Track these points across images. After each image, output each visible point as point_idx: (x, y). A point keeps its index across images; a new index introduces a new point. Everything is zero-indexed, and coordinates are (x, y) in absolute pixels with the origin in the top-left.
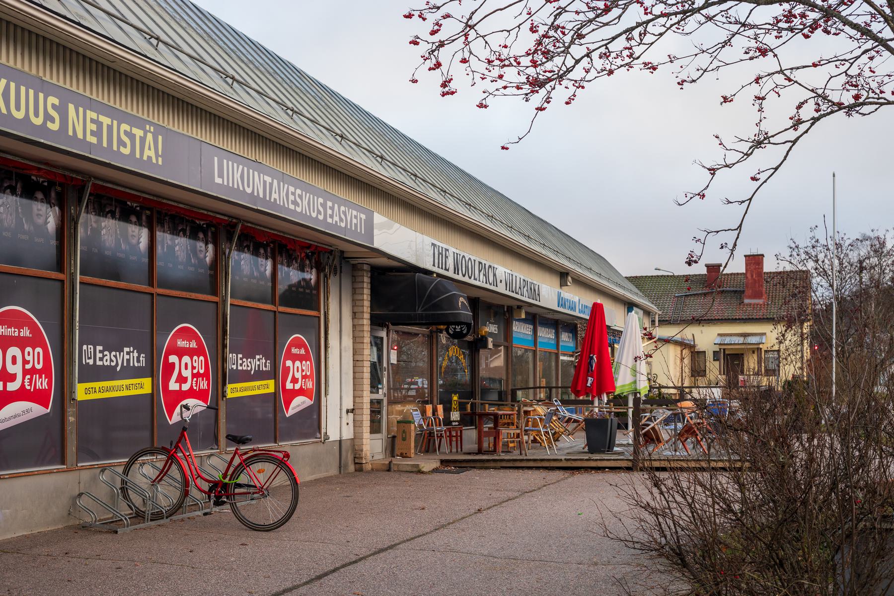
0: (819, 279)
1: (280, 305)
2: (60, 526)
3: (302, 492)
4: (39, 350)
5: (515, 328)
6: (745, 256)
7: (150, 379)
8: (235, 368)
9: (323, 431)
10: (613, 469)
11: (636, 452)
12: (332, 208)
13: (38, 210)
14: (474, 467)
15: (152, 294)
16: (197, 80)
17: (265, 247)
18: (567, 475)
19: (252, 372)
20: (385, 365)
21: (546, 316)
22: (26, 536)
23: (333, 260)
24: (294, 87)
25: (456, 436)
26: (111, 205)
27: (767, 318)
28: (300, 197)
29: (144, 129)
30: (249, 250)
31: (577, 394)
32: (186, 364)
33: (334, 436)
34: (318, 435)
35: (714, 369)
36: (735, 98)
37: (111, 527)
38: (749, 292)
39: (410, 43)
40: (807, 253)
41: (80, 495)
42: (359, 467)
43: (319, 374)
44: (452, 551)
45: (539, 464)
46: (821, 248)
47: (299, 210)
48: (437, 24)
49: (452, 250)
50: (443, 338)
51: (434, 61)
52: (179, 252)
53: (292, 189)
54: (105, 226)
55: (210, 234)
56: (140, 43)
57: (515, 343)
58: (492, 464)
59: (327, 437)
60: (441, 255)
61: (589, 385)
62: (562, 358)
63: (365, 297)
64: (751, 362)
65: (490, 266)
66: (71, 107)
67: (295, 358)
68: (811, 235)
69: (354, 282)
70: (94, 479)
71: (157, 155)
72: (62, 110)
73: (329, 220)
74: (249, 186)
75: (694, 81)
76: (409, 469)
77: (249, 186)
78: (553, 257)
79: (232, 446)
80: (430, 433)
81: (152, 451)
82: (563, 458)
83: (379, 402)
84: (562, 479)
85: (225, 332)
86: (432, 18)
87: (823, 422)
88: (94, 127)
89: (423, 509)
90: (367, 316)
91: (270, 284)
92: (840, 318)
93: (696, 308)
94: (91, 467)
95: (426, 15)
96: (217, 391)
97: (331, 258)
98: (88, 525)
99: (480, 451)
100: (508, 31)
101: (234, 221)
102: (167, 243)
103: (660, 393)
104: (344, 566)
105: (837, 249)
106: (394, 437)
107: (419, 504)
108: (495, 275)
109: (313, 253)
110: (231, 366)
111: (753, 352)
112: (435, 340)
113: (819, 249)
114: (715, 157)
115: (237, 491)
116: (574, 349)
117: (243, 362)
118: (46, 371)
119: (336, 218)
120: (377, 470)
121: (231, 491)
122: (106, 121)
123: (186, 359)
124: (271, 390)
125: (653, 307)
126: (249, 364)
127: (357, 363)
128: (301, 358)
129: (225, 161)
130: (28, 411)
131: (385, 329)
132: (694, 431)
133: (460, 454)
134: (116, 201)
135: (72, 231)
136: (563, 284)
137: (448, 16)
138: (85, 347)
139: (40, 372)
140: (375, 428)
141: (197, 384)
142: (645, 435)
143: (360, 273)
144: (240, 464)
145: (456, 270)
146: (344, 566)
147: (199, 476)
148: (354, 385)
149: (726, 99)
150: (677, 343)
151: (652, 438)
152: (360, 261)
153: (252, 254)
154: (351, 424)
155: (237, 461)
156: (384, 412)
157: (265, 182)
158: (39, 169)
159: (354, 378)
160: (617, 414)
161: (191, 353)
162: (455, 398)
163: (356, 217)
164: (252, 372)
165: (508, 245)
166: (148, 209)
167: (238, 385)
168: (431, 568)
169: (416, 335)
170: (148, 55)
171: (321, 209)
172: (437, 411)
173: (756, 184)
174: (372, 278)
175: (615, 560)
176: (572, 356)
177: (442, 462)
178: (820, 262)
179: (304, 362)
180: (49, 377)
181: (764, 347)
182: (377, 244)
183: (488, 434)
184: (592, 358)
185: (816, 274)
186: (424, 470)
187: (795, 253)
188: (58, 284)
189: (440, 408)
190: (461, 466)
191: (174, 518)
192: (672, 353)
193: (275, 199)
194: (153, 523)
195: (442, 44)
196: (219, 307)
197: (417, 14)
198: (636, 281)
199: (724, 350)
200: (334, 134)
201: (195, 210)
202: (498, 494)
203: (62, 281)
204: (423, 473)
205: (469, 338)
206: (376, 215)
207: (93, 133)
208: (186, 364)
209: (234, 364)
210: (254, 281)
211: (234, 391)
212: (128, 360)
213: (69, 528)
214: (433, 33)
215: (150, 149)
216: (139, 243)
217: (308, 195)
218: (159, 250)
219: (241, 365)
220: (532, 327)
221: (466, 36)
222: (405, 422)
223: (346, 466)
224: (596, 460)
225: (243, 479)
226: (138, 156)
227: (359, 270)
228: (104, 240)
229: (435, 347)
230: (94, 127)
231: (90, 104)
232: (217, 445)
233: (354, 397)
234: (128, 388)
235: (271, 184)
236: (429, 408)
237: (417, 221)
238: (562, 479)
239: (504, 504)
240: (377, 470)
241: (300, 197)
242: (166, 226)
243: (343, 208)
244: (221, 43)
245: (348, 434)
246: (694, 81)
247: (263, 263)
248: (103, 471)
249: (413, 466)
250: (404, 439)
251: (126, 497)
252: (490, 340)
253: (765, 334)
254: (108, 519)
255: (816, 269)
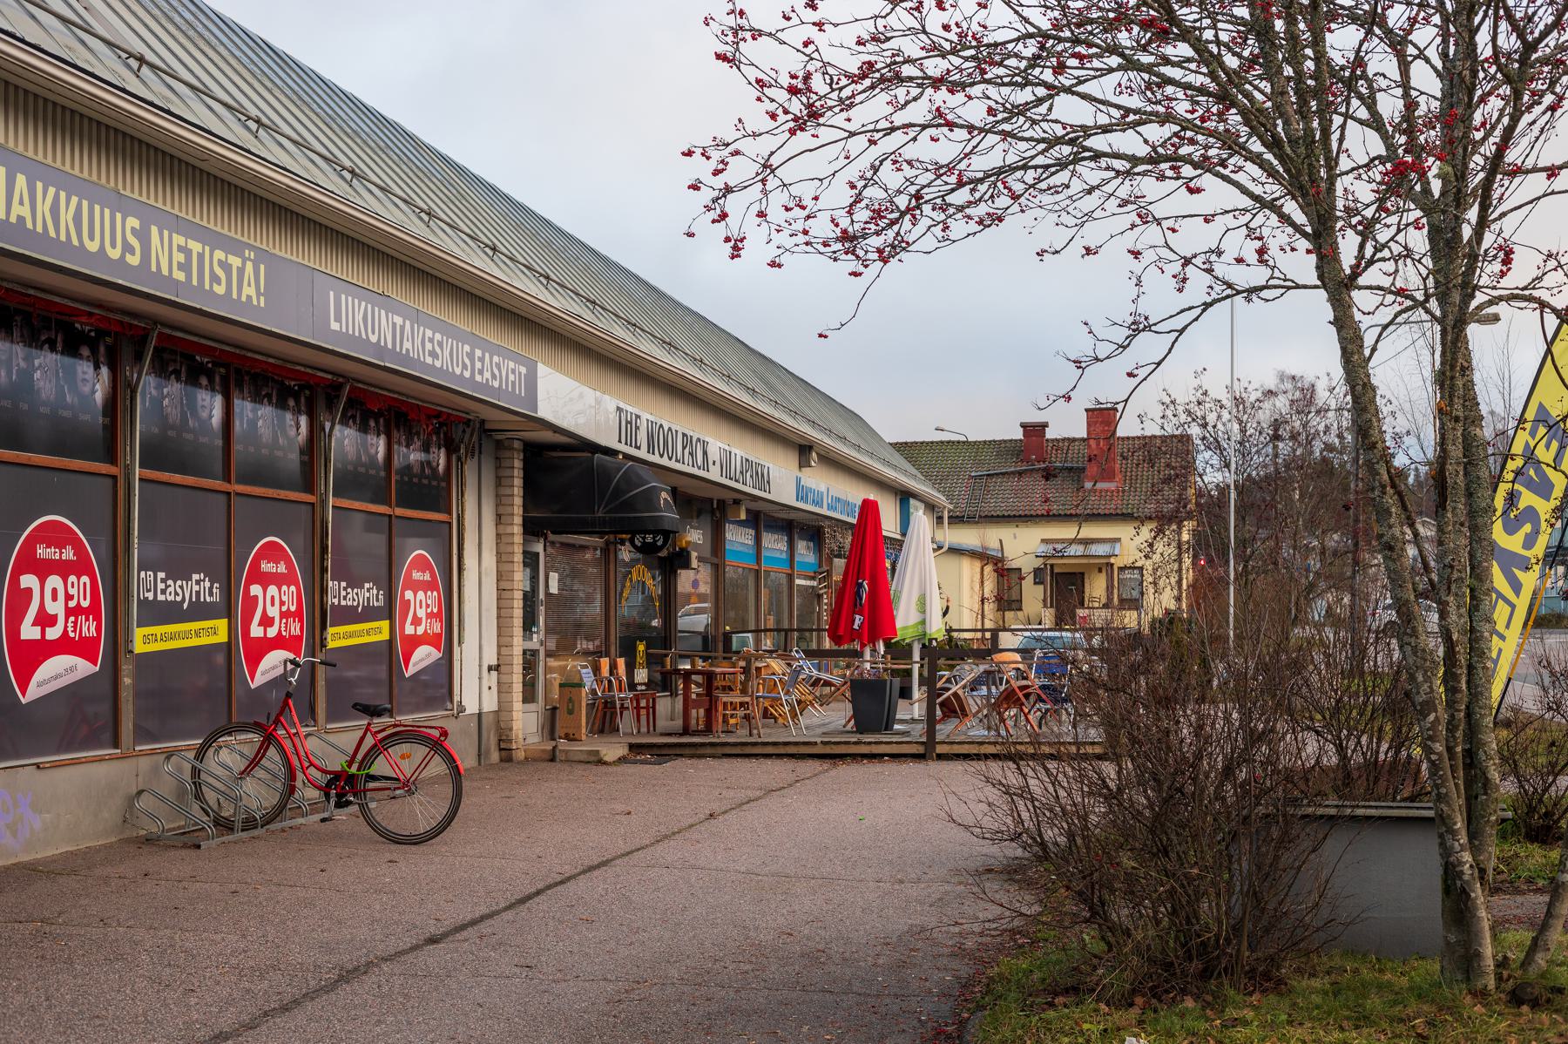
0: (1208, 454)
1: (398, 506)
2: (114, 839)
3: (466, 784)
4: (85, 579)
5: (728, 536)
6: (1087, 410)
7: (225, 621)
8: (151, 598)
9: (456, 698)
10: (895, 757)
11: (931, 732)
12: (482, 360)
13: (84, 373)
14: (681, 756)
15: (229, 494)
16: (240, 143)
17: (376, 417)
18: (826, 766)
19: (185, 606)
20: (542, 596)
21: (776, 515)
22: (72, 852)
23: (472, 435)
24: (414, 168)
25: (647, 708)
26: (175, 361)
27: (1123, 514)
28: (440, 344)
29: (241, 255)
30: (354, 423)
31: (836, 638)
32: (54, 591)
33: (471, 707)
34: (449, 707)
35: (1033, 596)
36: (1101, 251)
37: (190, 841)
38: (1093, 469)
39: (689, 187)
40: (1189, 413)
41: (140, 793)
42: (507, 755)
43: (448, 612)
44: (693, 867)
45: (782, 750)
46: (1212, 405)
47: (438, 364)
48: (722, 162)
49: (645, 416)
50: (626, 554)
51: (718, 211)
52: (42, 383)
53: (429, 333)
54: (40, 365)
55: (303, 399)
56: (237, 133)
57: (729, 558)
58: (709, 751)
59: (462, 709)
60: (629, 426)
61: (856, 627)
62: (798, 582)
63: (516, 491)
64: (1096, 588)
65: (699, 440)
66: (154, 230)
67: (266, 580)
68: (1197, 382)
69: (498, 467)
70: (155, 770)
71: (259, 294)
72: (143, 236)
73: (478, 378)
74: (92, 238)
75: (1057, 252)
76: (583, 757)
77: (92, 238)
78: (790, 421)
79: (362, 719)
80: (606, 702)
81: (243, 728)
82: (819, 740)
83: (534, 653)
84: (820, 773)
85: (324, 549)
86: (716, 155)
87: (1215, 683)
88: (180, 257)
89: (629, 813)
90: (518, 520)
91: (219, 442)
92: (1241, 517)
93: (1003, 496)
94: (152, 753)
95: (710, 152)
96: (314, 638)
97: (468, 431)
98: (154, 836)
99: (686, 731)
100: (821, 180)
101: (341, 380)
102: (18, 365)
103: (951, 639)
104: (549, 887)
105: (1237, 406)
106: (554, 709)
107: (620, 807)
108: (705, 453)
109: (441, 424)
110: (332, 600)
111: (1100, 570)
112: (612, 556)
113: (1207, 405)
114: (1083, 346)
115: (371, 785)
116: (816, 568)
117: (167, 587)
118: (93, 610)
119: (487, 375)
120: (535, 760)
121: (361, 786)
122: (195, 247)
123: (54, 581)
124: (222, 637)
125: (940, 499)
126: (179, 591)
127: (502, 593)
128: (278, 580)
129: (343, 297)
130: (72, 669)
131: (542, 540)
132: (1019, 699)
133: (655, 735)
134: (183, 355)
135: (128, 402)
136: (804, 463)
137: (737, 153)
138: (143, 574)
139: (85, 612)
140: (529, 697)
141: (75, 627)
142: (942, 705)
143: (507, 454)
144: (374, 746)
145: (651, 449)
146: (549, 887)
147: (312, 764)
148: (499, 627)
149: (1088, 251)
150: (973, 554)
151: (954, 709)
152: (509, 435)
153: (359, 431)
154: (495, 689)
155: (369, 741)
156: (541, 670)
157: (394, 325)
158: (90, 314)
159: (499, 617)
160: (894, 673)
161: (64, 569)
162: (641, 647)
163: (513, 371)
164: (185, 606)
165: (724, 405)
166: (222, 365)
167: (341, 629)
168: (673, 889)
169: (584, 548)
170: (80, 64)
171: (467, 361)
172: (616, 667)
173: (1134, 381)
174: (526, 461)
175: (927, 877)
176: (813, 578)
177: (632, 747)
178: (1210, 428)
179: (284, 588)
180: (98, 619)
181: (1118, 562)
182: (544, 411)
183: (697, 704)
184: (861, 585)
185: (1203, 447)
186: (606, 759)
187: (1169, 413)
188: (109, 482)
189: (621, 662)
190: (661, 753)
191: (272, 827)
192: (969, 570)
193: (408, 350)
194: (244, 834)
195: (728, 190)
196: (316, 510)
197: (699, 151)
198: (907, 450)
199: (1052, 566)
200: (339, 168)
201: (289, 366)
202: (731, 793)
203: (114, 477)
204: (605, 763)
205: (664, 553)
206: (540, 365)
207: (181, 267)
208: (54, 591)
209: (149, 591)
210: (362, 470)
211: (339, 637)
212: (198, 593)
213: (128, 841)
214: (716, 173)
215: (21, 203)
216: (211, 417)
217: (363, 304)
218: (238, 427)
219: (163, 592)
220: (752, 532)
221: (764, 181)
222: (571, 685)
223: (488, 752)
224: (870, 743)
225: (380, 767)
226: (235, 296)
227: (506, 448)
228: (39, 389)
229: (612, 567)
230: (180, 257)
231: (179, 225)
232: (315, 720)
233: (499, 646)
234: (198, 634)
235: (402, 328)
236: (605, 663)
237: (594, 372)
238: (820, 773)
239: (745, 807)
240: (535, 760)
241: (440, 344)
242: (16, 333)
243: (496, 359)
244: (315, 106)
245: (490, 704)
246: (1057, 252)
247: (205, 403)
248: (168, 758)
249: (590, 753)
250: (570, 712)
251: (199, 796)
252: (694, 555)
253: (1119, 540)
254: (179, 828)
255: (1204, 438)
